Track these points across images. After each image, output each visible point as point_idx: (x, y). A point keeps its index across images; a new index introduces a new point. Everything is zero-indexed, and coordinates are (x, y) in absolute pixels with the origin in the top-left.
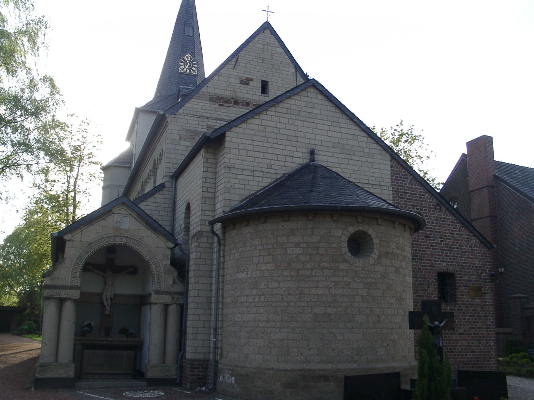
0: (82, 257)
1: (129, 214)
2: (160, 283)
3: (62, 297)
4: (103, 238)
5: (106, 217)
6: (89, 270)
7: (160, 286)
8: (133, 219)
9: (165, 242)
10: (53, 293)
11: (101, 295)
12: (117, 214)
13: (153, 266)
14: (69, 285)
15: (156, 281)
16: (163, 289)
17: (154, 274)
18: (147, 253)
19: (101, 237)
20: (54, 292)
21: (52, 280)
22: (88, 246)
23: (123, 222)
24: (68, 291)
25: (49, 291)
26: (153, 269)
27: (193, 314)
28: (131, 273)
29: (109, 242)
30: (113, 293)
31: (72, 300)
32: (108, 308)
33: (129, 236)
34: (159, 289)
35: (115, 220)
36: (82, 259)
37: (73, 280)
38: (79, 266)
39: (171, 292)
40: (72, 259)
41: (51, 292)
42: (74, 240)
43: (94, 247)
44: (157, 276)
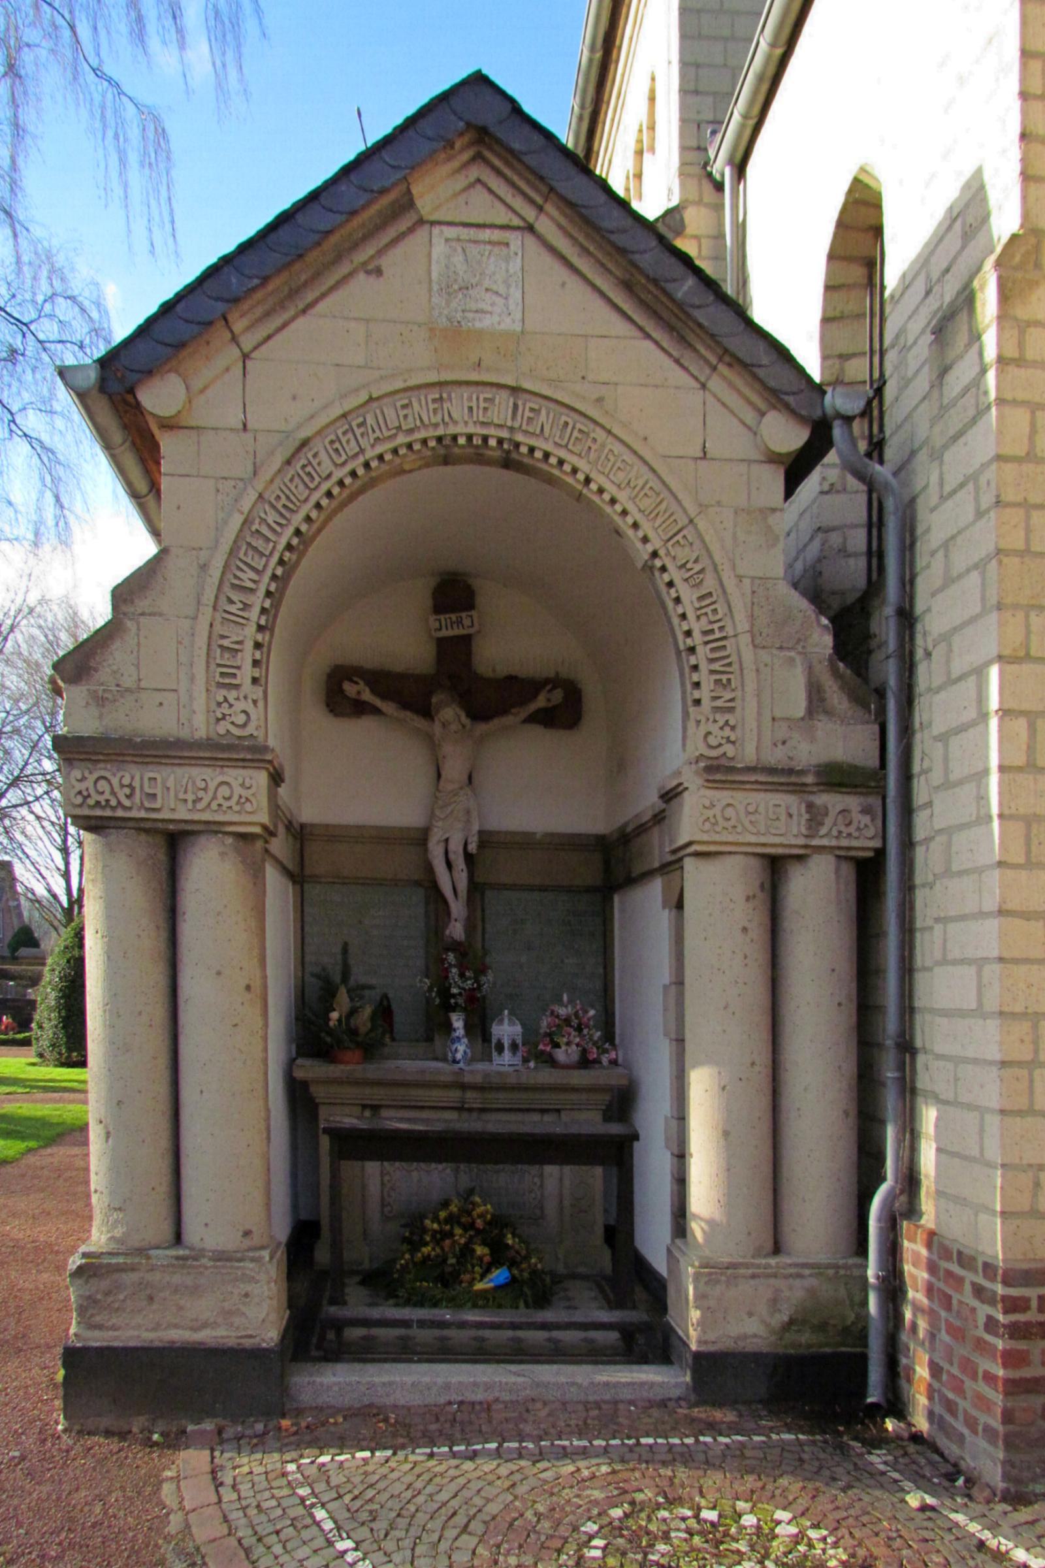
1: (516, 222)
2: (731, 710)
5: (380, 252)
6: (360, 709)
7: (733, 728)
8: (548, 260)
9: (750, 416)
10: (113, 793)
11: (420, 838)
13: (684, 591)
14: (201, 733)
15: (704, 694)
16: (749, 754)
17: (692, 650)
19: (363, 397)
20: (115, 782)
21: (100, 701)
22: (288, 462)
24: (200, 774)
25: (92, 778)
26: (683, 616)
27: (1001, 912)
28: (548, 719)
29: (411, 431)
30: (476, 828)
31: (229, 840)
32: (458, 908)
33: (527, 385)
34: (729, 750)
35: (434, 275)
36: (262, 554)
37: (219, 704)
38: (246, 606)
39: (802, 773)
40: (204, 555)
41: (102, 785)
42: (200, 423)
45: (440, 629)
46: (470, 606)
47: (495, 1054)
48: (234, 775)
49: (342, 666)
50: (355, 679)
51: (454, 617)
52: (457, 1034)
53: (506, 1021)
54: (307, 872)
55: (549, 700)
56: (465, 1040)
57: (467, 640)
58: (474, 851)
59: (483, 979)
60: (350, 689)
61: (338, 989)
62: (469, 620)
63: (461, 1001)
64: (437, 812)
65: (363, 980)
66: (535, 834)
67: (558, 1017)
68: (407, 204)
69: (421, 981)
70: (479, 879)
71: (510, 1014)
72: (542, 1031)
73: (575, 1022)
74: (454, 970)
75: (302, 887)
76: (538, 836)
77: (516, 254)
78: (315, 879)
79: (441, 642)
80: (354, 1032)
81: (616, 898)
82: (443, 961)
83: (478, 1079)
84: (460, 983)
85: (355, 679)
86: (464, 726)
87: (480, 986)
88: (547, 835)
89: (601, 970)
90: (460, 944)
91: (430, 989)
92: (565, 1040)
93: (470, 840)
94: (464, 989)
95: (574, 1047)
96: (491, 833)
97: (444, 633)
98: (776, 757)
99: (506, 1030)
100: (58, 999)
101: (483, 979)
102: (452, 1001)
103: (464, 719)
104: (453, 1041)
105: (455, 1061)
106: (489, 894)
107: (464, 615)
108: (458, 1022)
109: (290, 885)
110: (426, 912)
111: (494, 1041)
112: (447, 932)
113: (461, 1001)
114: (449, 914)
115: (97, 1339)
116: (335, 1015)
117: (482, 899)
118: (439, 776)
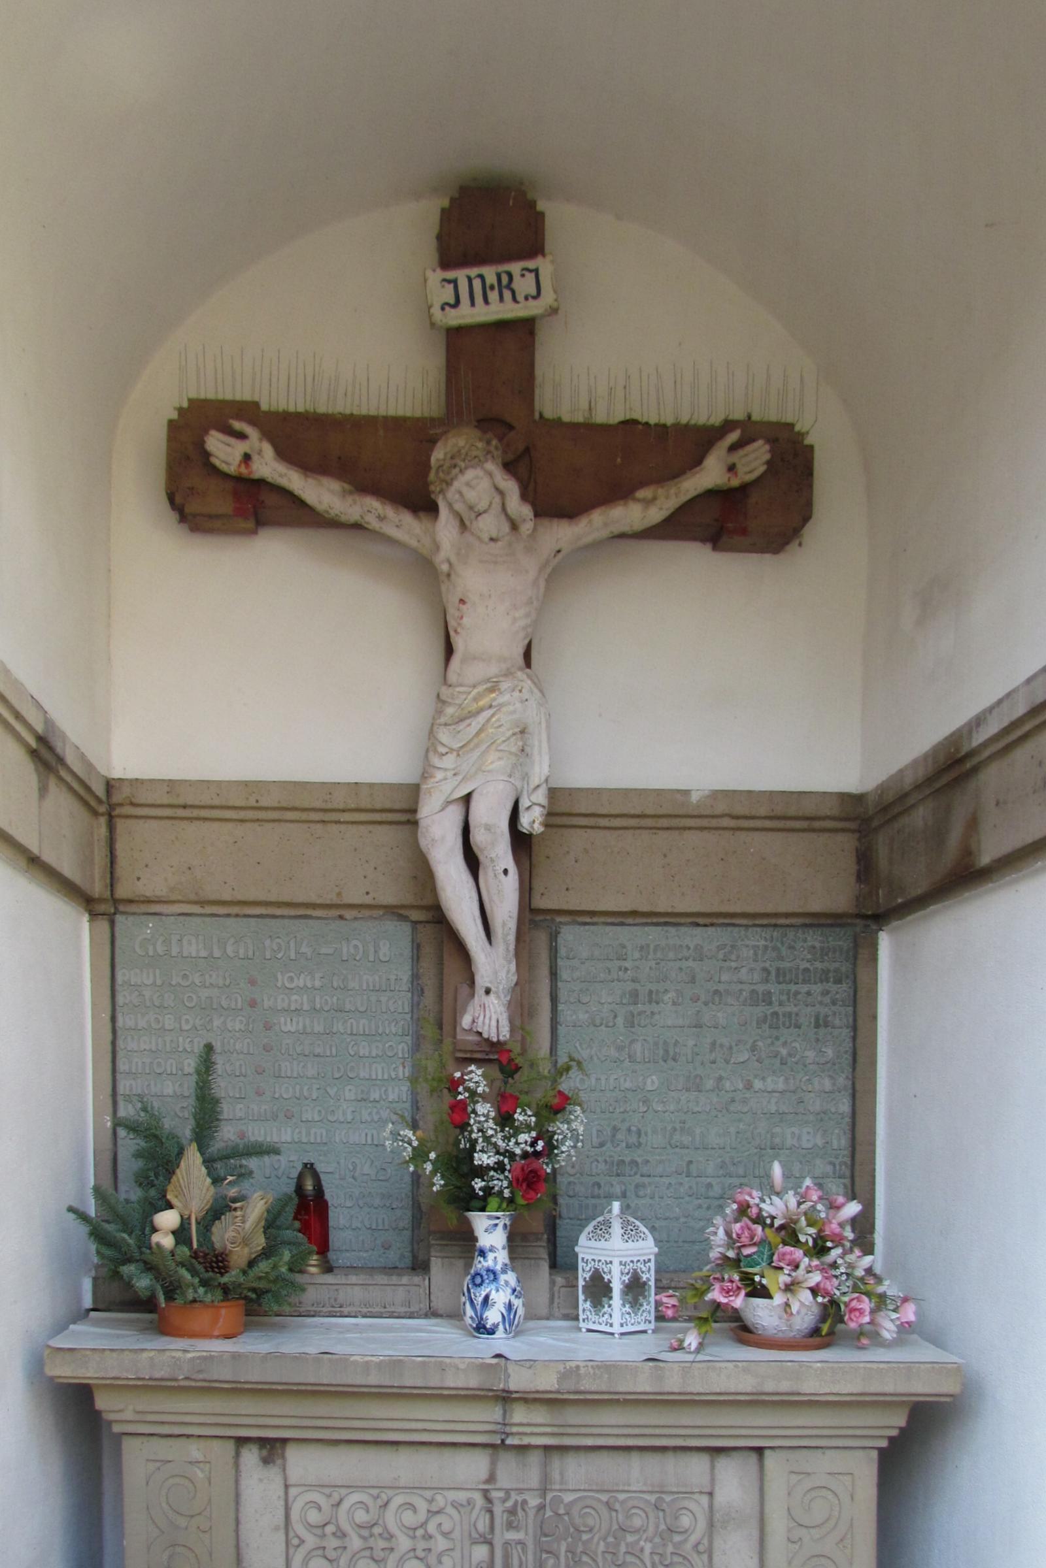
45: (457, 303)
46: (535, 248)
47: (584, 1305)
49: (206, 402)
50: (238, 425)
51: (490, 273)
52: (489, 1262)
53: (617, 1228)
54: (122, 892)
55: (732, 468)
56: (511, 1277)
57: (525, 329)
58: (538, 828)
59: (560, 1128)
61: (181, 1152)
62: (531, 277)
63: (500, 1183)
64: (444, 736)
65: (258, 1133)
66: (687, 793)
67: (759, 1220)
69: (395, 1135)
70: (540, 903)
71: (625, 1209)
72: (714, 1254)
73: (807, 1235)
74: (483, 1108)
75: (112, 923)
76: (694, 798)
77: (506, 872)
78: (146, 904)
79: (456, 336)
80: (217, 1262)
81: (885, 942)
82: (454, 1085)
83: (547, 1382)
84: (499, 1140)
85: (238, 425)
86: (514, 526)
87: (551, 1147)
88: (716, 795)
89: (845, 1107)
90: (496, 1046)
91: (419, 1155)
92: (783, 1278)
93: (524, 803)
94: (512, 1156)
95: (806, 1296)
96: (571, 792)
97: (469, 314)
101: (560, 1128)
102: (478, 1184)
103: (521, 510)
104: (478, 1280)
105: (482, 1328)
106: (569, 935)
107: (515, 268)
109: (86, 918)
110: (415, 977)
111: (583, 1276)
112: (466, 1021)
113: (500, 1183)
114: (471, 981)
117: (554, 952)
118: (449, 650)
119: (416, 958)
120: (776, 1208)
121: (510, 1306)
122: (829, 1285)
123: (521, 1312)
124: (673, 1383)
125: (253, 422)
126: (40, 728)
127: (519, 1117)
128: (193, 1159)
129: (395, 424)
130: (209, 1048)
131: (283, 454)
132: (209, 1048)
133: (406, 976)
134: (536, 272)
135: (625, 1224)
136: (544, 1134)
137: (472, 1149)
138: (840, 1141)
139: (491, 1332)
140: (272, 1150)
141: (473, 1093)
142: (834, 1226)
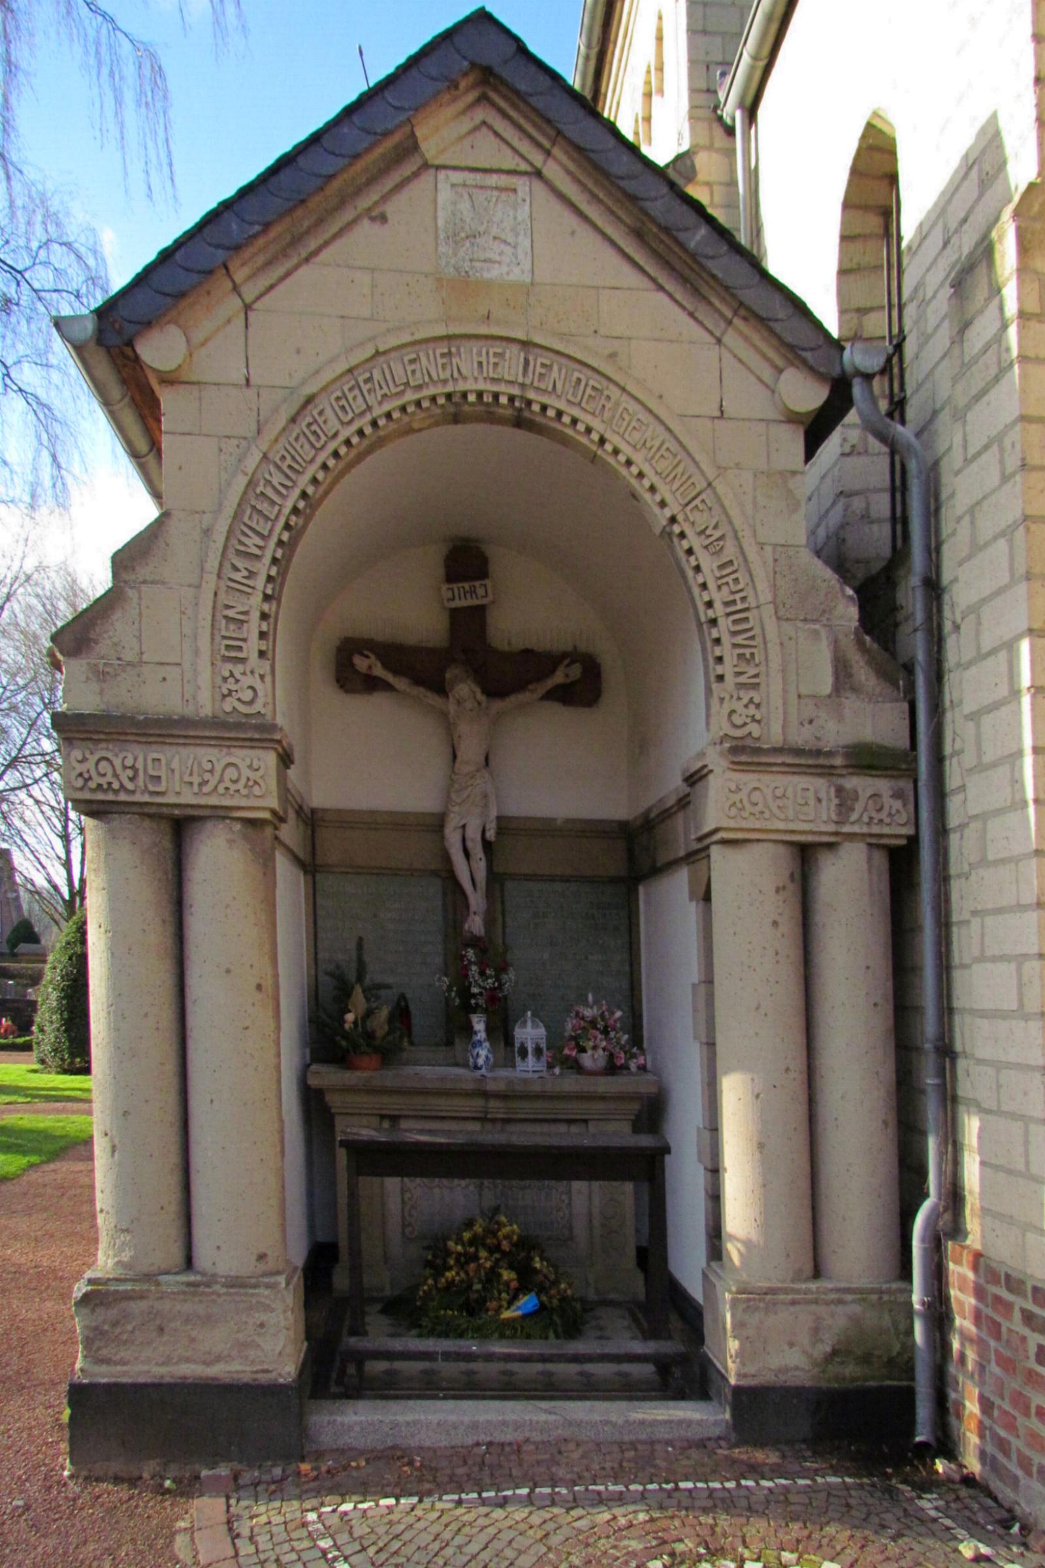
0: (264, 507)
1: (524, 167)
2: (755, 686)
3: (170, 799)
4: (378, 353)
5: (385, 198)
6: (371, 684)
7: (758, 706)
8: (558, 208)
10: (116, 775)
11: (436, 824)
12: (456, 177)
14: (207, 711)
16: (775, 734)
18: (662, 466)
19: (369, 351)
20: (117, 763)
21: (101, 676)
22: (293, 420)
23: (495, 231)
24: (207, 755)
25: (93, 759)
26: (704, 586)
29: (419, 387)
30: (494, 813)
32: (477, 900)
34: (755, 729)
35: (441, 223)
37: (225, 679)
38: (252, 574)
40: (207, 519)
43: (333, 425)
44: (735, 633)
47: (518, 1059)
48: (242, 757)
50: (366, 652)
51: (467, 586)
53: (529, 1024)
55: (567, 676)
56: (487, 1044)
57: (480, 611)
58: (493, 839)
59: (504, 977)
60: (361, 663)
61: (353, 988)
63: (481, 1001)
64: (454, 796)
67: (583, 1018)
68: (411, 147)
70: (499, 869)
71: (533, 1015)
72: (566, 1034)
73: (601, 1025)
74: (474, 968)
75: (314, 877)
79: (454, 613)
80: (370, 1036)
81: (641, 889)
82: (462, 957)
84: (480, 981)
85: (366, 652)
86: (479, 703)
87: (501, 985)
88: (568, 821)
89: (627, 968)
91: (450, 988)
92: (591, 1044)
93: (488, 827)
94: (485, 988)
95: (600, 1052)
97: (457, 604)
98: (801, 737)
99: (529, 1033)
100: (60, 999)
101: (504, 977)
102: (473, 1001)
103: (480, 696)
104: (474, 1046)
105: (477, 1067)
106: (509, 885)
107: (477, 584)
108: (479, 1024)
111: (517, 1045)
112: (466, 926)
113: (481, 1001)
115: (105, 1375)
116: (350, 1017)
117: (502, 891)
118: (455, 756)
119: (445, 894)
120: (588, 1013)
121: (487, 1057)
122: (609, 1047)
123: (492, 1060)
124: (549, 1087)
125: (371, 650)
126: (299, 800)
127: (488, 972)
128: (358, 990)
129: (432, 651)
130: (361, 939)
131: (386, 666)
132: (361, 939)
133: (440, 903)
134: (485, 586)
135: (533, 1022)
136: (498, 979)
137: (470, 986)
138: (625, 984)
139: (480, 1068)
140: (388, 987)
141: (469, 961)
142: (612, 1022)
